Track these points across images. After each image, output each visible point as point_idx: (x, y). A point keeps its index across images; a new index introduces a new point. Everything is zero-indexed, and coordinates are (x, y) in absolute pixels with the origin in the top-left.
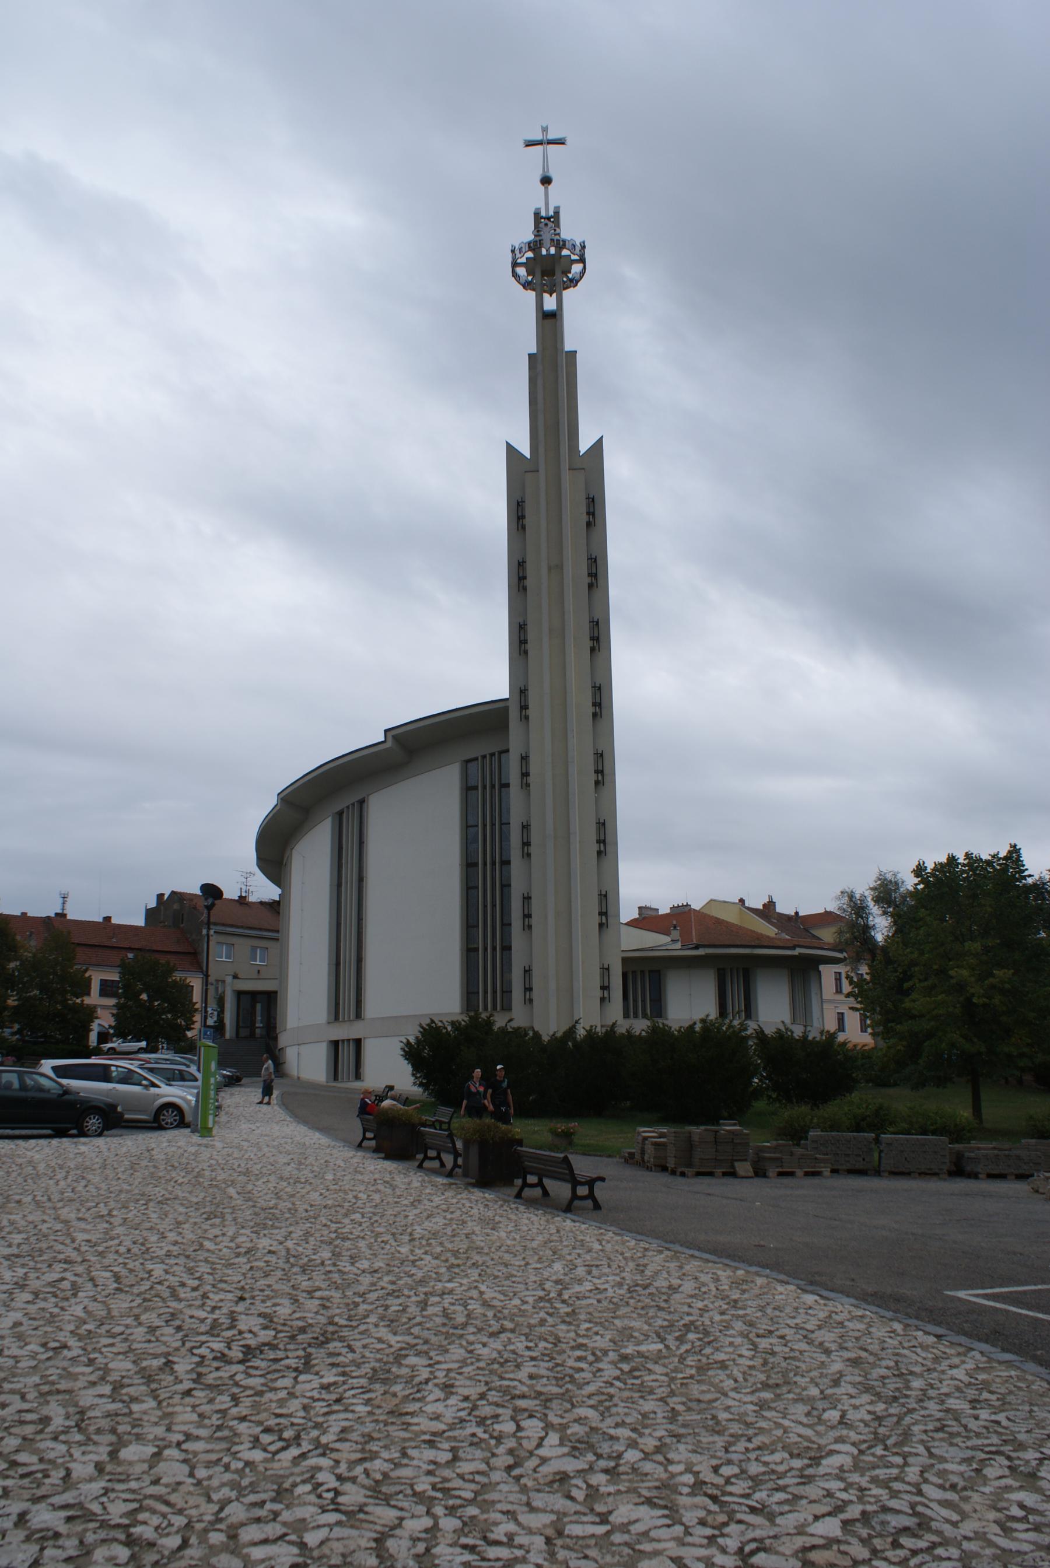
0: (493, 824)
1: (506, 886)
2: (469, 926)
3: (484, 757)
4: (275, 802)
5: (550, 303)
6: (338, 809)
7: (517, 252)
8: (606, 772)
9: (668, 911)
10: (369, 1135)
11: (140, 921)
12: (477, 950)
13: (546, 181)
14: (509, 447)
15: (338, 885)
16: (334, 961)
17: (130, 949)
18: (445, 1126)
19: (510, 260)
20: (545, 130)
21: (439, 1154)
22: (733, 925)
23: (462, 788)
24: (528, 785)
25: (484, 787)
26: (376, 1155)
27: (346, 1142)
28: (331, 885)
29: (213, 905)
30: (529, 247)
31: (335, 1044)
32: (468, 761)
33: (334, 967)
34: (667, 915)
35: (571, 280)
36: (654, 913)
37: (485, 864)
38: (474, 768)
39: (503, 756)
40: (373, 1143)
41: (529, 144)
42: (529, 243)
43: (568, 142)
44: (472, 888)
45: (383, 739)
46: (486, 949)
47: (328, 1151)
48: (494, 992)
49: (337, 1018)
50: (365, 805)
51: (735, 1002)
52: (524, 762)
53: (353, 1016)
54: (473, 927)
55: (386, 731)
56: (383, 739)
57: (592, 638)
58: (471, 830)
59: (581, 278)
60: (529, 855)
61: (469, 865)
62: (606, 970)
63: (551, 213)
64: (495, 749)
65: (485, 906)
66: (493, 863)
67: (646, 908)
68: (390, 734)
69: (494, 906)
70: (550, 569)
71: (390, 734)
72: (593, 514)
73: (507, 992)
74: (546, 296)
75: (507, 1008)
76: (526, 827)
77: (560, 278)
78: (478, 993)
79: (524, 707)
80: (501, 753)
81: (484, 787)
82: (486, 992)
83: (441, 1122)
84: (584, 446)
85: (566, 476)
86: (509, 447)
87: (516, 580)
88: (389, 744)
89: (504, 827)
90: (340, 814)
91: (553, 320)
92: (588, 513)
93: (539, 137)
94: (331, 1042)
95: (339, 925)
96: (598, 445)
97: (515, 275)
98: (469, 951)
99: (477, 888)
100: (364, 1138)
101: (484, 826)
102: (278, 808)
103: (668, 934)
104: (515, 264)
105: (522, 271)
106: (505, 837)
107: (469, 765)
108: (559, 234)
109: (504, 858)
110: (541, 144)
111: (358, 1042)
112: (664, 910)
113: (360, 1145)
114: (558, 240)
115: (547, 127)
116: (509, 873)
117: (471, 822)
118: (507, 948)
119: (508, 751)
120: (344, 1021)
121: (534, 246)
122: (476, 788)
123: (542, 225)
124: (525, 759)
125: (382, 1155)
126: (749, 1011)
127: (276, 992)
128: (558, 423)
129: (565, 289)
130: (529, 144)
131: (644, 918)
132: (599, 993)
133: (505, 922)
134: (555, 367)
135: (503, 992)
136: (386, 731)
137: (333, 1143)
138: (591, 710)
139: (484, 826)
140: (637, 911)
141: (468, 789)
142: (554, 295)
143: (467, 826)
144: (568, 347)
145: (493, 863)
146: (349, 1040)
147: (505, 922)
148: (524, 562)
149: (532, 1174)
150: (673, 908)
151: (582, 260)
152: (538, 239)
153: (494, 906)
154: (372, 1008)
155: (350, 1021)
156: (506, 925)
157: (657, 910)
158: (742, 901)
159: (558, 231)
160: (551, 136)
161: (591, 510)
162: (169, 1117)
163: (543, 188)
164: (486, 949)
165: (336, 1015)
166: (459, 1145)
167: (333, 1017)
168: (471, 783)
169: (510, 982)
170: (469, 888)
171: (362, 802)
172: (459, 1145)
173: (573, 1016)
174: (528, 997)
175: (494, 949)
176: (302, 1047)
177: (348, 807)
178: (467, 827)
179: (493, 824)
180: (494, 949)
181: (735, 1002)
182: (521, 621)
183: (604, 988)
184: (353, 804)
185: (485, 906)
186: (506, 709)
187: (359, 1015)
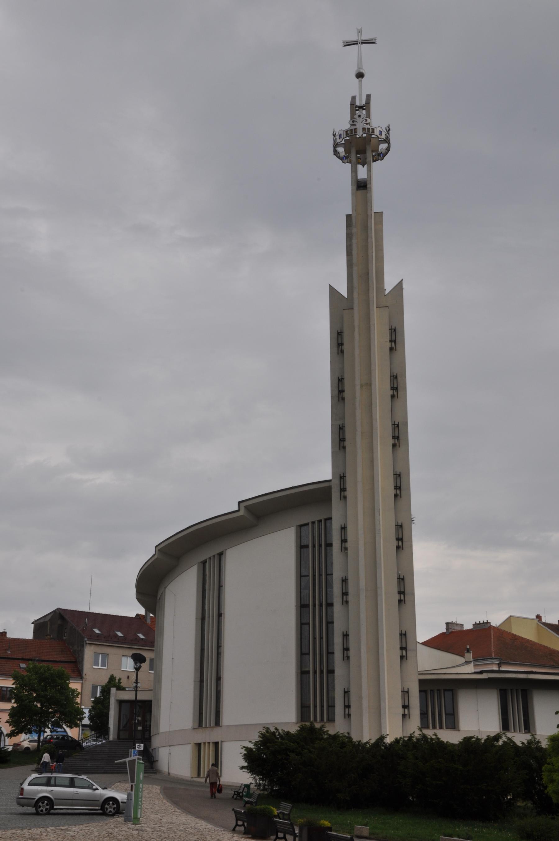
0: (320, 575)
1: (330, 623)
2: (302, 654)
3: (313, 523)
4: (153, 553)
5: (362, 172)
6: (203, 559)
7: (337, 137)
8: (405, 539)
9: (471, 627)
10: (240, 823)
11: (28, 634)
12: (308, 672)
13: (360, 75)
14: (332, 289)
15: (202, 618)
16: (198, 679)
17: (23, 660)
18: (286, 817)
19: (332, 142)
20: (359, 32)
21: (285, 836)
22: (528, 641)
23: (297, 547)
24: (346, 549)
25: (314, 546)
26: (244, 836)
27: (225, 828)
28: (197, 619)
29: (140, 667)
30: (347, 134)
31: (199, 745)
32: (301, 526)
33: (198, 684)
34: (470, 630)
35: (379, 154)
36: (458, 628)
37: (314, 605)
38: (305, 530)
39: (328, 522)
40: (242, 828)
41: (348, 44)
42: (347, 132)
43: (377, 41)
44: (305, 654)
45: (237, 509)
46: (315, 672)
47: (216, 833)
48: (322, 706)
49: (200, 725)
50: (223, 557)
51: (516, 716)
52: (343, 531)
53: (213, 724)
54: (305, 654)
55: (239, 503)
56: (237, 509)
57: (394, 437)
58: (303, 578)
59: (387, 153)
60: (347, 602)
61: (302, 606)
62: (406, 693)
63: (364, 103)
64: (322, 517)
65: (315, 638)
66: (321, 605)
67: (452, 623)
68: (243, 505)
69: (321, 638)
70: (362, 386)
71: (246, 507)
72: (395, 341)
73: (331, 707)
74: (360, 167)
75: (331, 720)
76: (345, 581)
77: (370, 155)
78: (310, 707)
79: (343, 490)
80: (326, 520)
81: (314, 546)
82: (315, 707)
83: (284, 814)
84: (389, 285)
85: (375, 313)
86: (332, 289)
87: (337, 392)
88: (242, 513)
89: (329, 577)
90: (204, 563)
91: (364, 191)
92: (391, 341)
93: (354, 38)
94: (196, 744)
95: (202, 650)
96: (399, 287)
97: (336, 153)
98: (303, 673)
99: (308, 624)
100: (237, 825)
101: (314, 576)
102: (156, 557)
103: (463, 656)
104: (336, 145)
105: (341, 150)
106: (329, 585)
107: (303, 528)
108: (369, 124)
109: (329, 601)
110: (357, 44)
111: (216, 744)
112: (468, 626)
113: (234, 830)
114: (369, 129)
115: (361, 29)
116: (333, 612)
117: (304, 573)
118: (331, 672)
119: (331, 518)
120: (206, 727)
121: (351, 133)
122: (307, 546)
123: (356, 116)
124: (343, 529)
125: (250, 836)
126: (528, 726)
127: (150, 702)
128: (368, 274)
129: (374, 161)
130: (348, 44)
131: (452, 632)
132: (401, 711)
133: (330, 651)
134: (366, 228)
135: (328, 706)
136: (239, 503)
137: (216, 829)
138: (393, 492)
139: (314, 576)
140: (444, 627)
141: (301, 547)
142: (366, 166)
143: (301, 576)
144: (376, 208)
145: (321, 605)
146: (209, 743)
147: (330, 651)
148: (343, 379)
149: (281, 832)
150: (475, 625)
151: (387, 140)
152: (353, 128)
153: (321, 638)
154: (227, 719)
155: (210, 727)
156: (330, 653)
157: (462, 625)
158: (539, 617)
159: (369, 121)
160: (364, 38)
161: (393, 338)
162: (110, 808)
163: (357, 80)
164: (315, 672)
165: (200, 723)
166: (297, 831)
167: (197, 725)
168: (304, 543)
169: (334, 698)
170: (302, 624)
171: (221, 554)
172: (297, 831)
173: (381, 732)
174: (347, 712)
175: (322, 672)
176: (172, 747)
177: (210, 558)
178: (301, 576)
179: (320, 575)
180: (322, 672)
181: (516, 716)
182: (340, 423)
183: (405, 707)
184: (214, 556)
185: (315, 638)
186: (329, 489)
187: (218, 722)
